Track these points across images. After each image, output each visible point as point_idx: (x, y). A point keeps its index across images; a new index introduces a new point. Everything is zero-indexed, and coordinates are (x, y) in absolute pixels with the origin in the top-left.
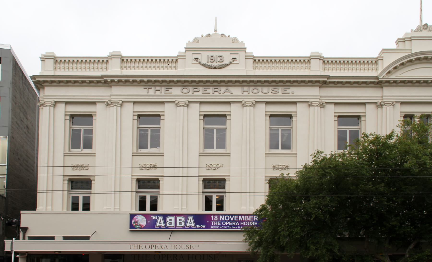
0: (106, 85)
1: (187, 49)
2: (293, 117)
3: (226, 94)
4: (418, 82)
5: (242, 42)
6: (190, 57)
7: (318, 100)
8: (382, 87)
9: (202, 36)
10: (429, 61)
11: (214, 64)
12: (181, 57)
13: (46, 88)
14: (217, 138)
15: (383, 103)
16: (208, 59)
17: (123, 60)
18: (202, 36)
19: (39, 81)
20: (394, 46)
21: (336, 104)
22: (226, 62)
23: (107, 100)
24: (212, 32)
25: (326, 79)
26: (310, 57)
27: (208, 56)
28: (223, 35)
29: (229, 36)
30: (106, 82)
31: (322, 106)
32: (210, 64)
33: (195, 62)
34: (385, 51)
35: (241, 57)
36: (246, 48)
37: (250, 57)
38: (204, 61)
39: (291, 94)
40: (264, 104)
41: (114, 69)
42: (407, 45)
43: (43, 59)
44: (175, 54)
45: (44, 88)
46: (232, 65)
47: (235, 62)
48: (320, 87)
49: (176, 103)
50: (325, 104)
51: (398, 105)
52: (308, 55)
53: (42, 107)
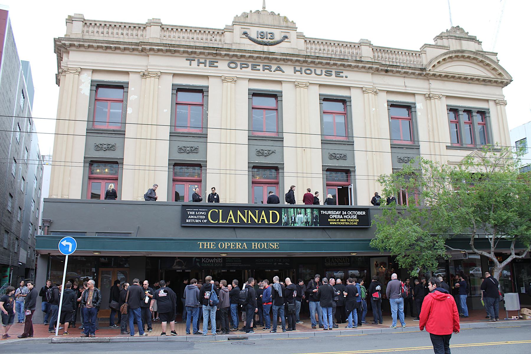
0: (142, 53)
1: (235, 23)
2: (348, 103)
3: (277, 72)
4: (453, 77)
5: (293, 21)
6: (238, 30)
7: (372, 87)
8: (428, 80)
9: (251, 11)
10: (411, 76)
11: (265, 40)
12: (229, 29)
13: (71, 53)
14: (43, 212)
15: (431, 95)
16: (258, 36)
17: (163, 28)
18: (251, 11)
19: (65, 44)
20: (433, 43)
21: (388, 92)
22: (277, 38)
23: (144, 71)
24: (261, 9)
25: (378, 66)
26: (360, 44)
27: (258, 32)
28: (272, 13)
29: (279, 14)
30: (142, 49)
31: (376, 93)
32: (259, 39)
33: (244, 36)
34: (426, 46)
35: (292, 35)
36: (297, 28)
37: (300, 36)
38: (254, 36)
39: (344, 78)
40: (318, 87)
41: (153, 35)
42: (445, 42)
43: (70, 20)
44: (221, 26)
45: (68, 53)
46: (283, 43)
47: (286, 40)
48: (372, 74)
49: (223, 78)
50: (378, 91)
51: (444, 99)
52: (357, 41)
53: (63, 74)
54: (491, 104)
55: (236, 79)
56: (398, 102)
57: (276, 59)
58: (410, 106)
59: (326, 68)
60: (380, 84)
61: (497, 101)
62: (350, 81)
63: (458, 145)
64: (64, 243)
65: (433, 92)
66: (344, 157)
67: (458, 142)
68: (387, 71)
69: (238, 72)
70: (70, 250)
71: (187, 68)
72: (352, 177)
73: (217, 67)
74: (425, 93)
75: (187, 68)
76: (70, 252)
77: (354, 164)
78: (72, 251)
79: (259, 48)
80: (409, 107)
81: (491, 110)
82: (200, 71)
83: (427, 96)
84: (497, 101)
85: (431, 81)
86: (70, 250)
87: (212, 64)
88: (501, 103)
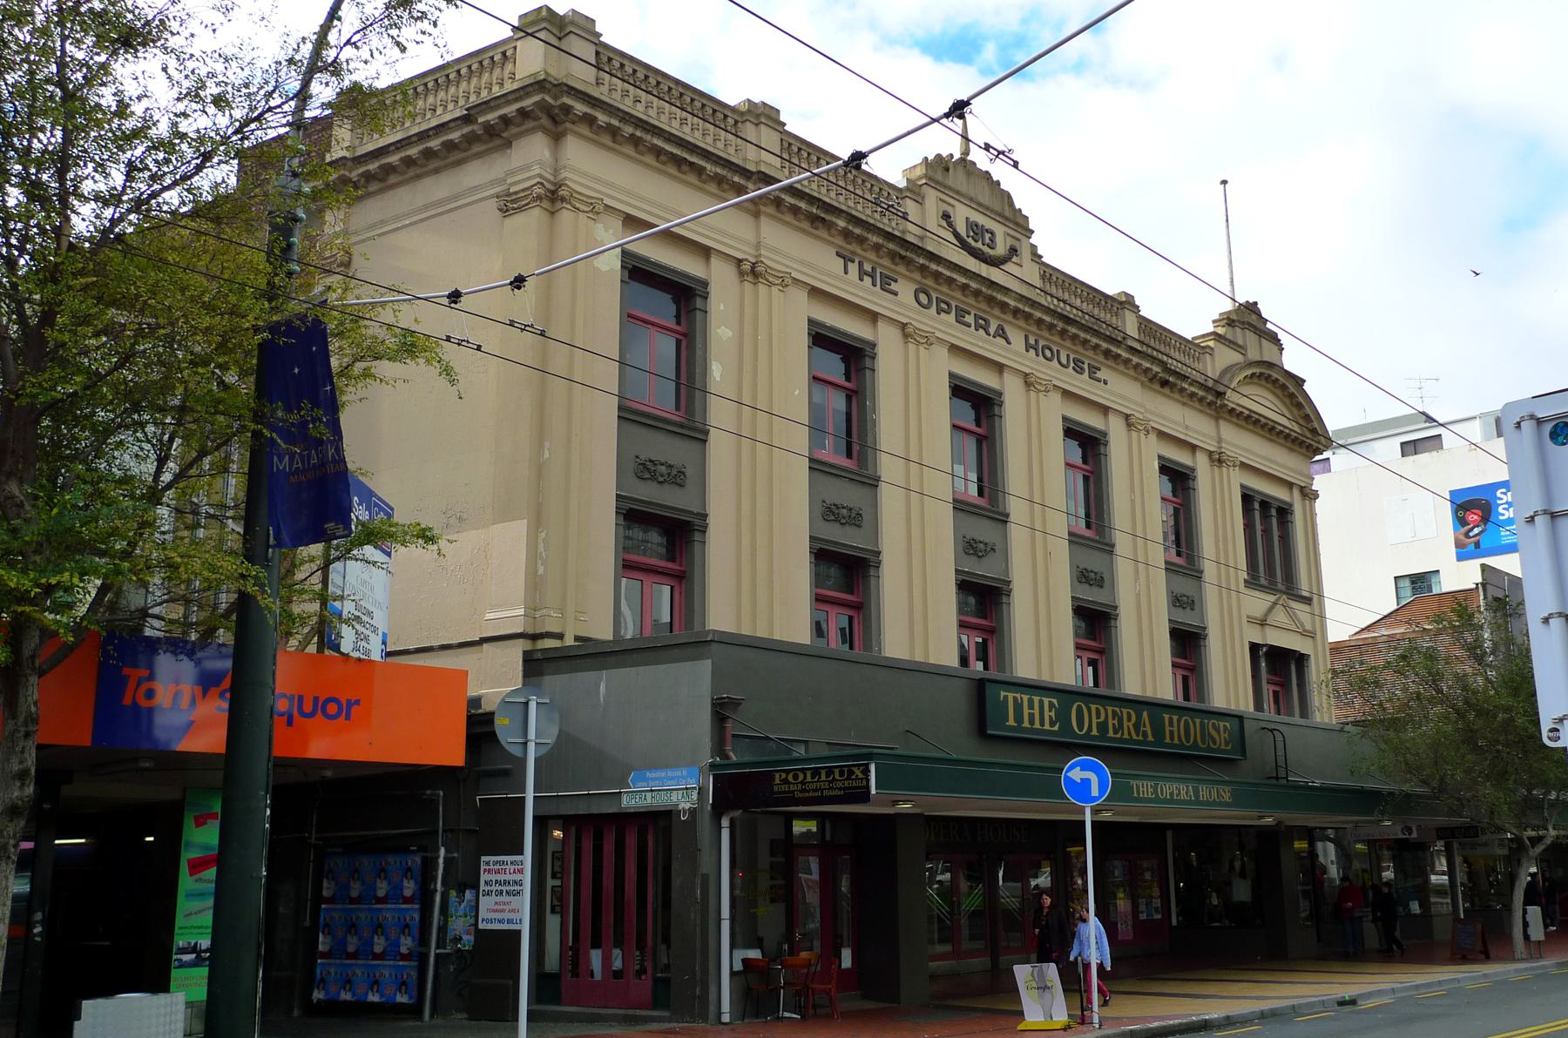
15: (759, 269)
54: (1296, 492)
55: (600, 208)
56: (674, 271)
57: (1003, 306)
58: (861, 350)
59: (1076, 352)
60: (585, 174)
61: (910, 330)
62: (1113, 394)
63: (841, 461)
64: (1077, 774)
65: (770, 260)
66: (676, 478)
67: (678, 409)
68: (1165, 383)
69: (945, 326)
70: (1095, 792)
71: (836, 277)
72: (873, 581)
73: (896, 294)
74: (740, 256)
75: (836, 277)
76: (1096, 799)
77: (1203, 621)
78: (1101, 795)
79: (972, 264)
80: (686, 296)
81: (713, 290)
82: (624, 198)
83: (746, 267)
84: (910, 330)
85: (1222, 423)
86: (1095, 792)
87: (886, 283)
88: (1309, 495)
